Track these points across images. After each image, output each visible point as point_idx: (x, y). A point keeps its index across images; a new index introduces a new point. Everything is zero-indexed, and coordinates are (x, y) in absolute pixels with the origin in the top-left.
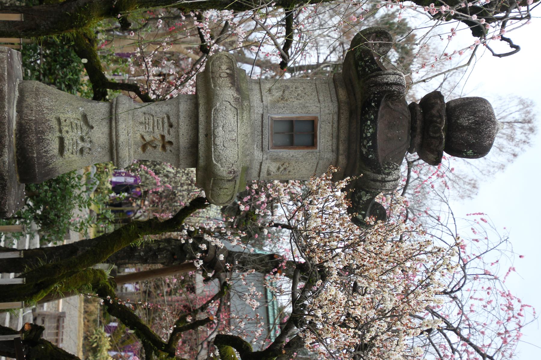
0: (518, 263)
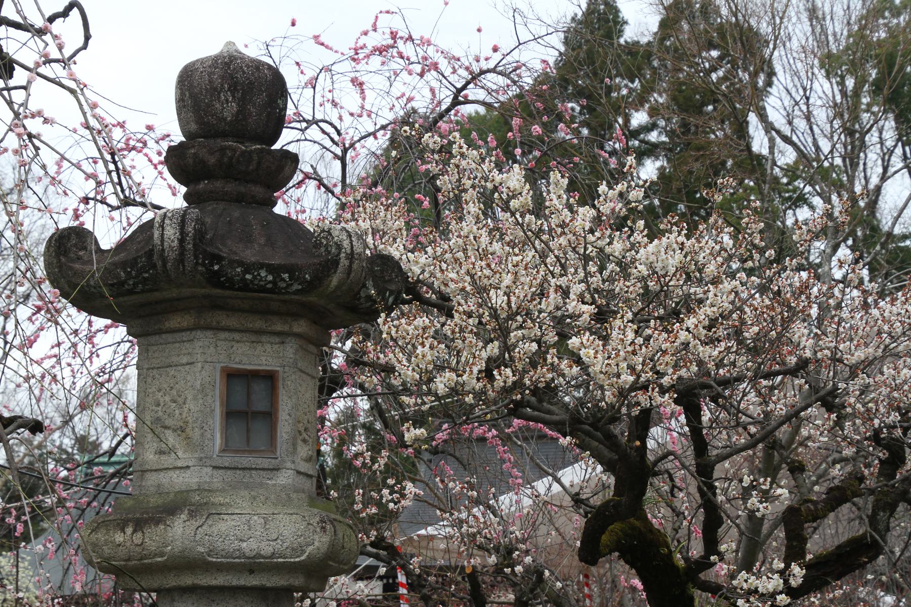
0: (306, 29)
